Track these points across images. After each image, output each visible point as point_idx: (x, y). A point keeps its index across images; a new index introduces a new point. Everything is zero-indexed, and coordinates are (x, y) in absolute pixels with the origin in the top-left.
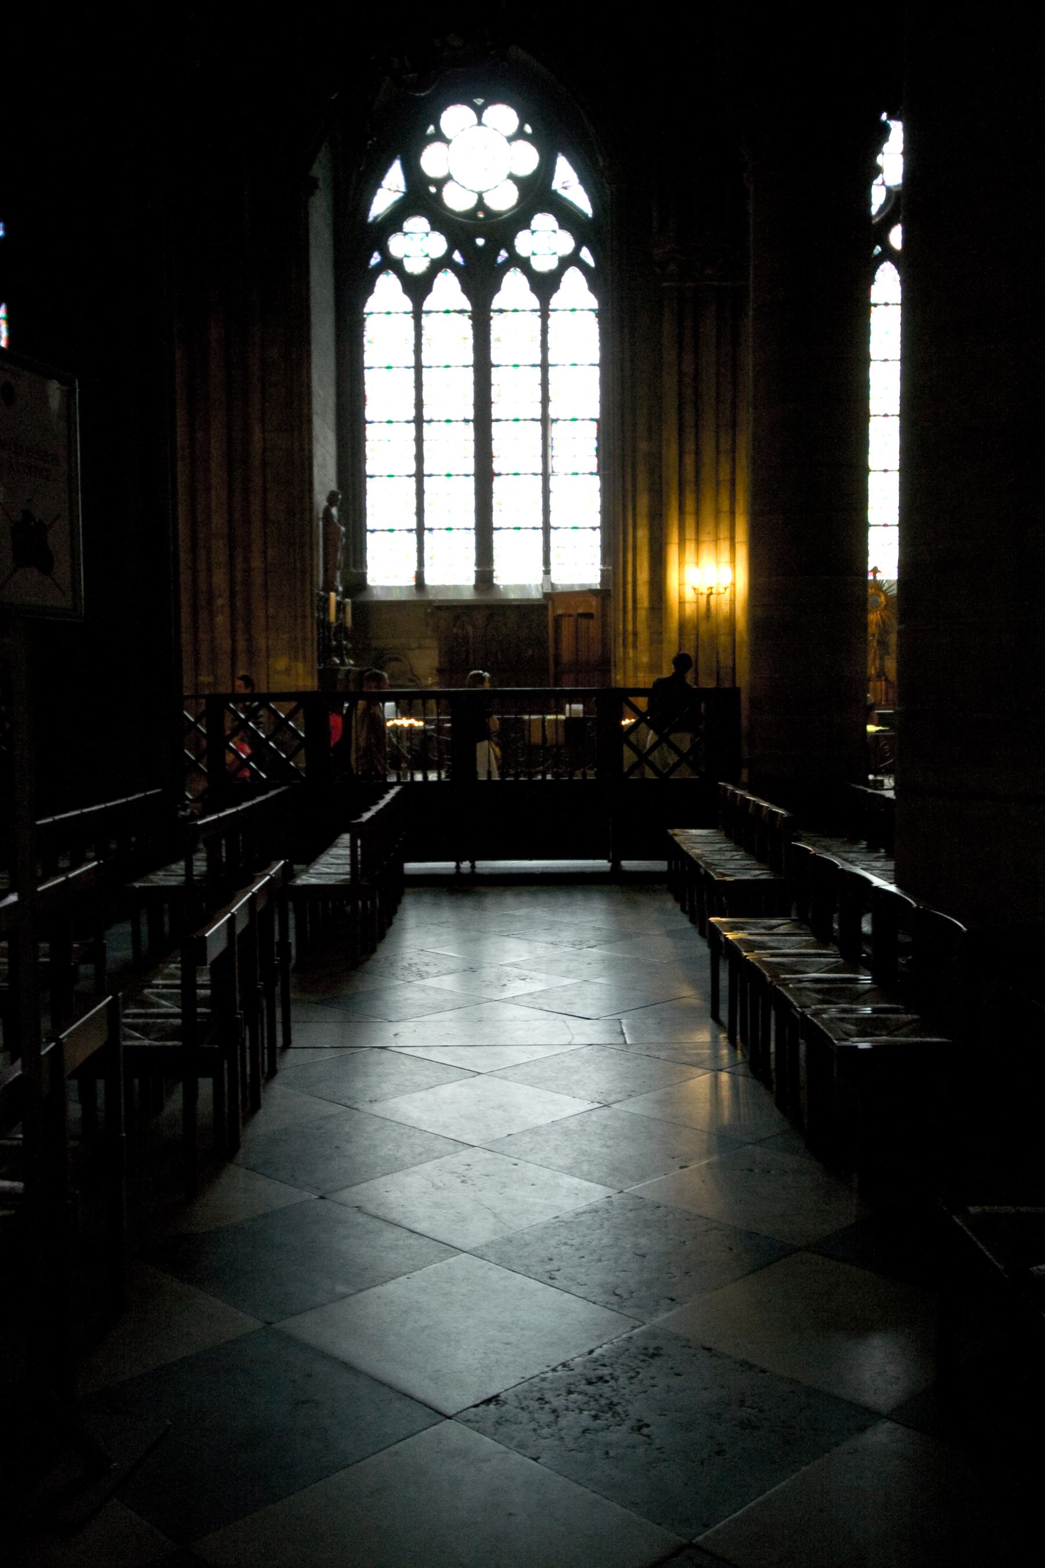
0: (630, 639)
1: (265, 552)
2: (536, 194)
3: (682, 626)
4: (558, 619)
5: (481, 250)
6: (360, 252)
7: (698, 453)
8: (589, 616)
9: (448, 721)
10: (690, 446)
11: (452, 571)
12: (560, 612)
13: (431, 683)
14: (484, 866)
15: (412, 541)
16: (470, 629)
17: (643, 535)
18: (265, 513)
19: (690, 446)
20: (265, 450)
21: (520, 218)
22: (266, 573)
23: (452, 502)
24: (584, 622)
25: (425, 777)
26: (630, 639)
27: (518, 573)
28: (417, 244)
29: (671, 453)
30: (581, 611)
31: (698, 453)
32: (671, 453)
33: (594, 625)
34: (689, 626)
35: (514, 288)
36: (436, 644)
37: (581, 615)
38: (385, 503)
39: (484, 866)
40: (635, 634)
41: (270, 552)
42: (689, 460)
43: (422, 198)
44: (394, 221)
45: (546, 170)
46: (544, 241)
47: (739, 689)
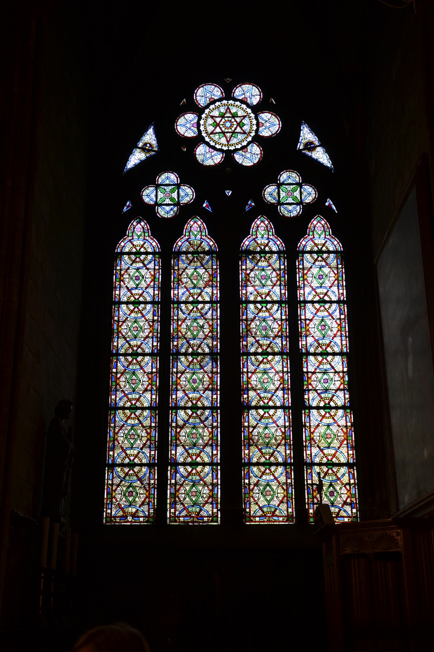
2: (280, 153)
5: (229, 198)
6: (114, 201)
9: (244, 461)
11: (196, 498)
14: (170, 440)
15: (152, 466)
21: (267, 172)
23: (196, 439)
27: (269, 499)
28: (167, 194)
35: (261, 234)
38: (130, 439)
39: (170, 440)
43: (177, 154)
44: (147, 173)
45: (289, 133)
46: (290, 193)
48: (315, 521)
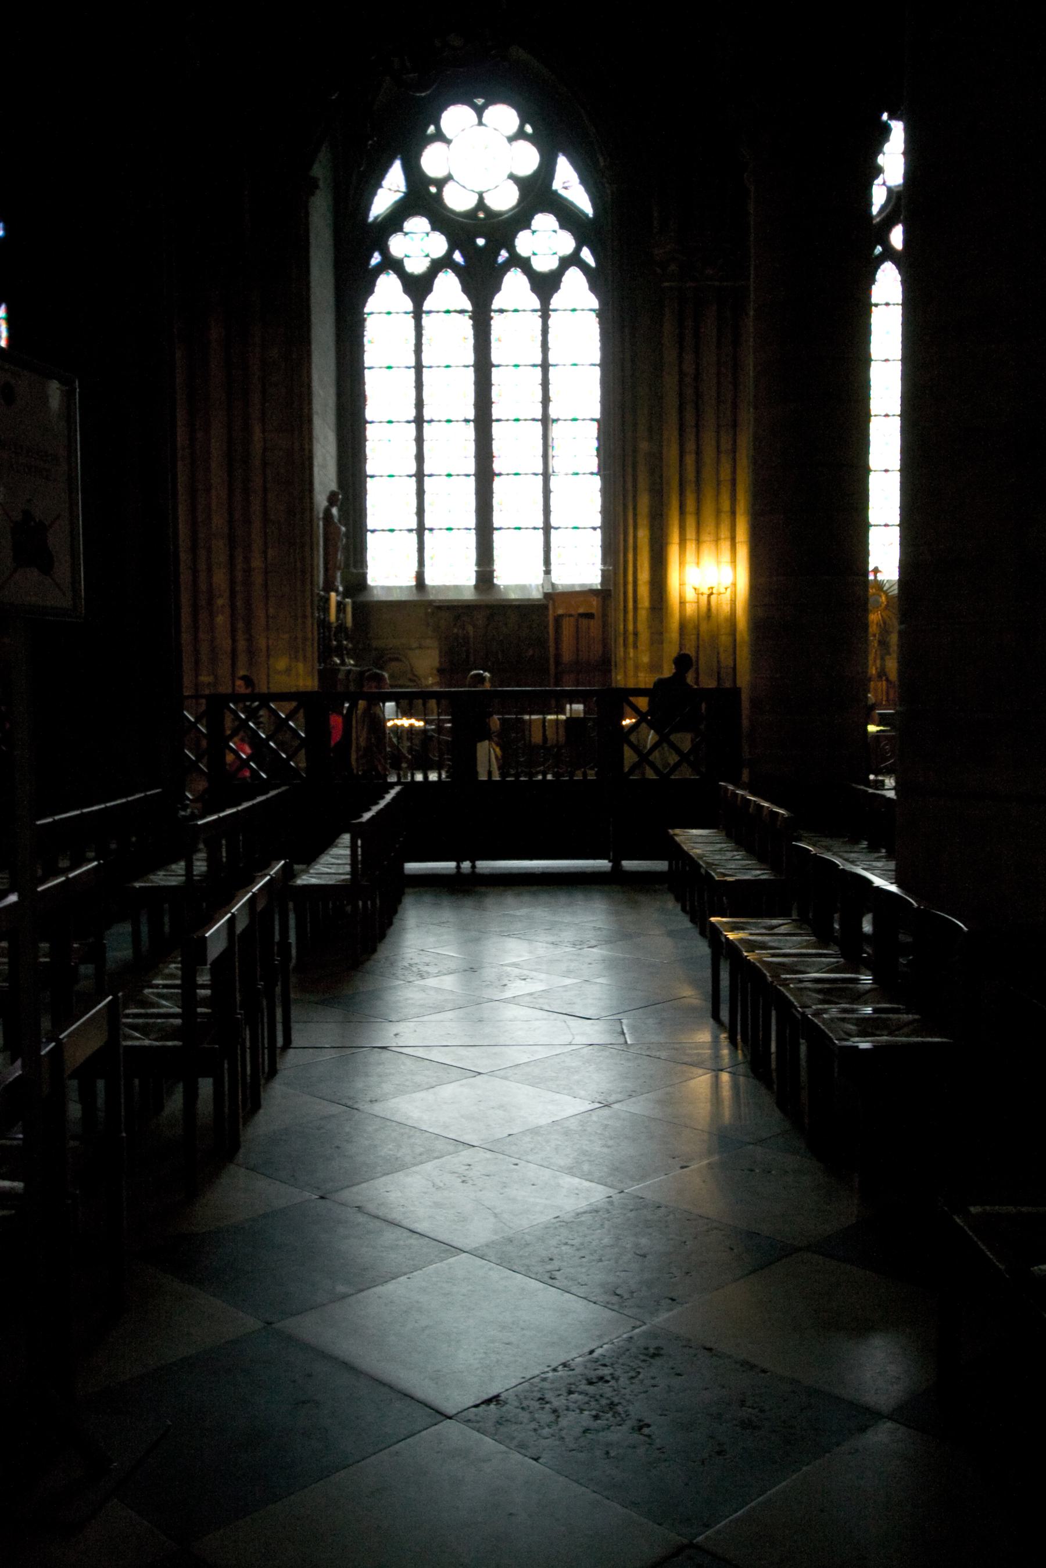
0: (631, 639)
1: (265, 552)
2: (537, 194)
3: (682, 626)
4: (558, 619)
5: (481, 250)
6: (360, 252)
7: (698, 453)
8: (589, 616)
10: (691, 446)
11: (453, 571)
12: (560, 612)
13: (431, 683)
14: (485, 866)
15: (412, 541)
16: (470, 629)
17: (643, 535)
18: (265, 513)
19: (691, 446)
20: (265, 450)
21: (521, 218)
22: (266, 573)
23: (453, 502)
24: (584, 622)
25: (426, 777)
26: (631, 639)
27: (518, 573)
28: (418, 244)
29: (672, 453)
30: (581, 611)
31: (698, 453)
32: (672, 453)
33: (595, 625)
34: (690, 626)
35: (514, 288)
36: (436, 644)
37: (582, 615)
38: (386, 503)
39: (485, 866)
40: (636, 634)
41: (270, 552)
42: (690, 460)
43: (422, 198)
44: (394, 221)
45: (547, 170)
46: (545, 241)
47: (740, 689)
48: (439, 769)
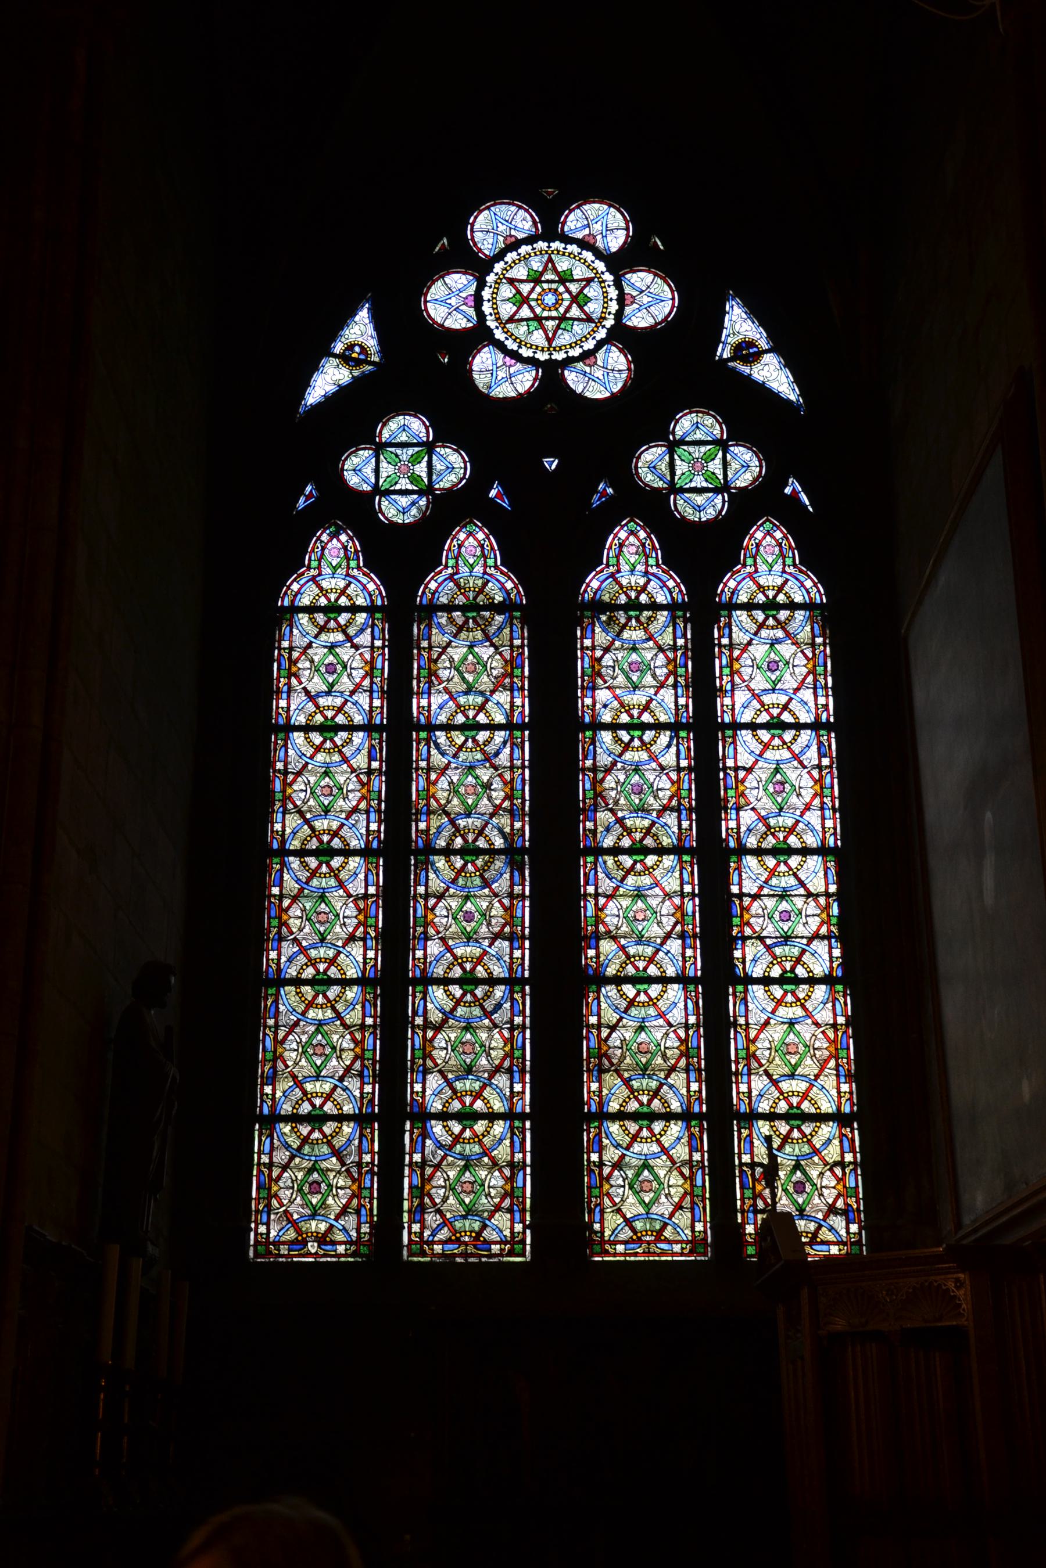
2: (675, 368)
5: (552, 477)
6: (275, 484)
11: (474, 1198)
14: (409, 1058)
15: (366, 1120)
21: (643, 413)
23: (473, 1055)
25: (751, 1244)
27: (647, 1199)
28: (402, 465)
35: (630, 562)
38: (313, 1056)
39: (409, 1058)
43: (426, 371)
44: (355, 417)
45: (697, 320)
46: (699, 463)
